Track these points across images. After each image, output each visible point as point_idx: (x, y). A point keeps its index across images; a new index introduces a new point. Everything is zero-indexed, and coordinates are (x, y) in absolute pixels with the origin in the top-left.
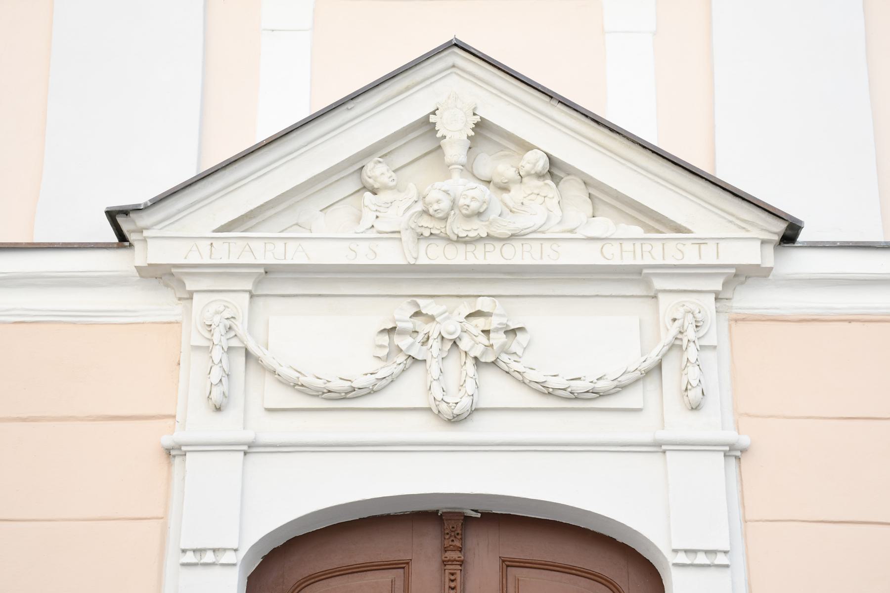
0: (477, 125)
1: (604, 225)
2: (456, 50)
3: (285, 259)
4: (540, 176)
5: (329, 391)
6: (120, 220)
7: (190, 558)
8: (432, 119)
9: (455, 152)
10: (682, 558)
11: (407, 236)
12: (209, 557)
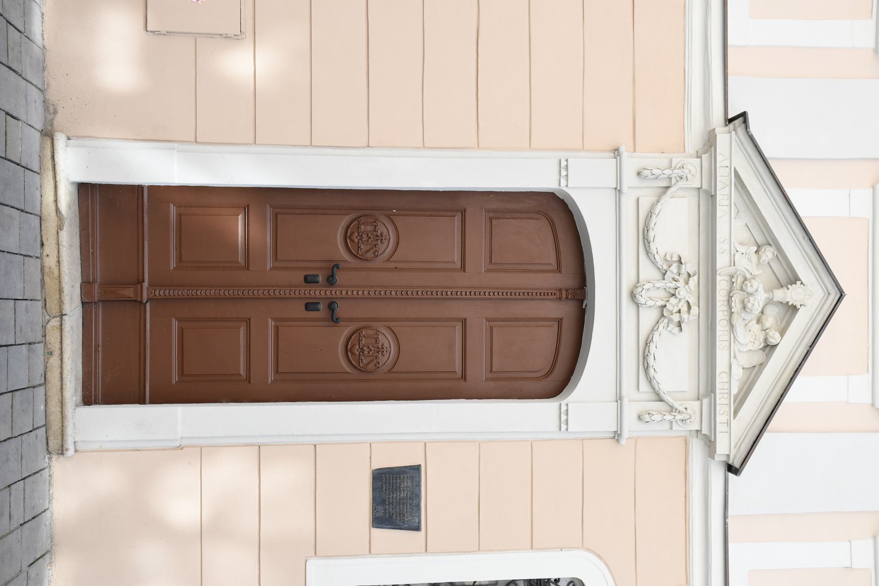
0: (795, 307)
1: (738, 374)
2: (839, 295)
3: (315, 446)
4: (766, 340)
5: (648, 230)
6: (741, 119)
7: (564, 163)
8: (798, 283)
9: (780, 295)
10: (564, 408)
11: (732, 270)
12: (564, 173)
